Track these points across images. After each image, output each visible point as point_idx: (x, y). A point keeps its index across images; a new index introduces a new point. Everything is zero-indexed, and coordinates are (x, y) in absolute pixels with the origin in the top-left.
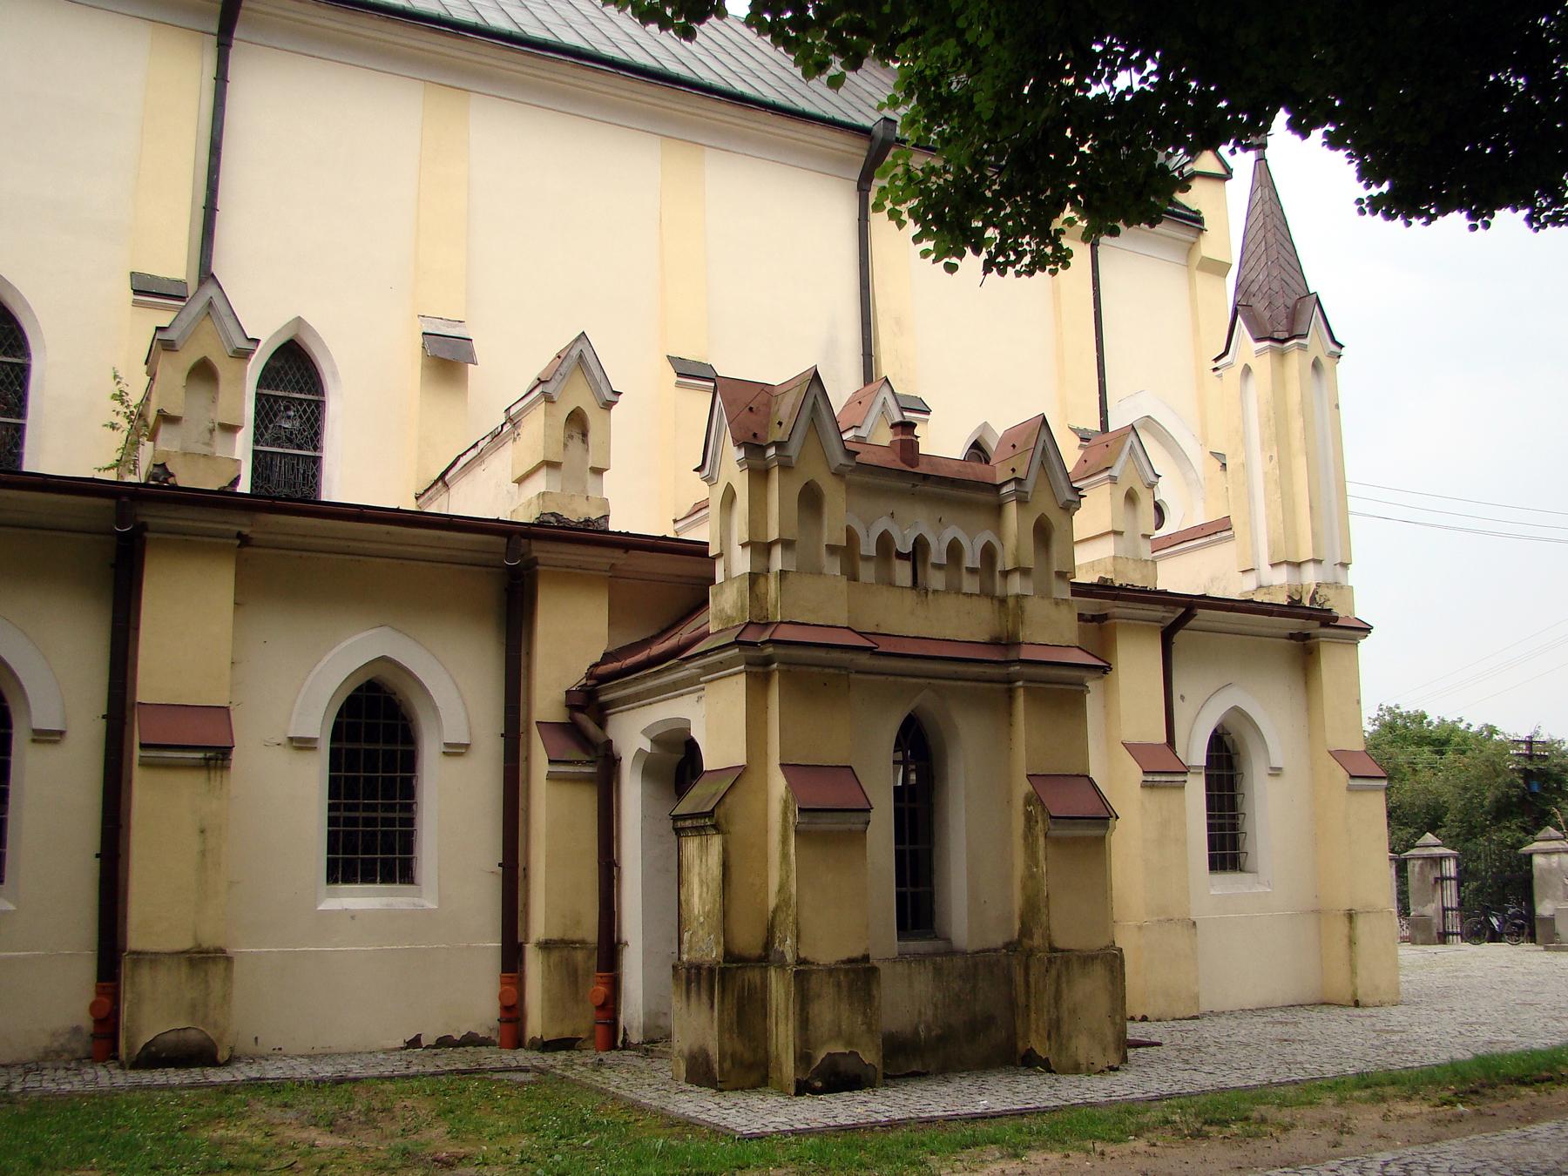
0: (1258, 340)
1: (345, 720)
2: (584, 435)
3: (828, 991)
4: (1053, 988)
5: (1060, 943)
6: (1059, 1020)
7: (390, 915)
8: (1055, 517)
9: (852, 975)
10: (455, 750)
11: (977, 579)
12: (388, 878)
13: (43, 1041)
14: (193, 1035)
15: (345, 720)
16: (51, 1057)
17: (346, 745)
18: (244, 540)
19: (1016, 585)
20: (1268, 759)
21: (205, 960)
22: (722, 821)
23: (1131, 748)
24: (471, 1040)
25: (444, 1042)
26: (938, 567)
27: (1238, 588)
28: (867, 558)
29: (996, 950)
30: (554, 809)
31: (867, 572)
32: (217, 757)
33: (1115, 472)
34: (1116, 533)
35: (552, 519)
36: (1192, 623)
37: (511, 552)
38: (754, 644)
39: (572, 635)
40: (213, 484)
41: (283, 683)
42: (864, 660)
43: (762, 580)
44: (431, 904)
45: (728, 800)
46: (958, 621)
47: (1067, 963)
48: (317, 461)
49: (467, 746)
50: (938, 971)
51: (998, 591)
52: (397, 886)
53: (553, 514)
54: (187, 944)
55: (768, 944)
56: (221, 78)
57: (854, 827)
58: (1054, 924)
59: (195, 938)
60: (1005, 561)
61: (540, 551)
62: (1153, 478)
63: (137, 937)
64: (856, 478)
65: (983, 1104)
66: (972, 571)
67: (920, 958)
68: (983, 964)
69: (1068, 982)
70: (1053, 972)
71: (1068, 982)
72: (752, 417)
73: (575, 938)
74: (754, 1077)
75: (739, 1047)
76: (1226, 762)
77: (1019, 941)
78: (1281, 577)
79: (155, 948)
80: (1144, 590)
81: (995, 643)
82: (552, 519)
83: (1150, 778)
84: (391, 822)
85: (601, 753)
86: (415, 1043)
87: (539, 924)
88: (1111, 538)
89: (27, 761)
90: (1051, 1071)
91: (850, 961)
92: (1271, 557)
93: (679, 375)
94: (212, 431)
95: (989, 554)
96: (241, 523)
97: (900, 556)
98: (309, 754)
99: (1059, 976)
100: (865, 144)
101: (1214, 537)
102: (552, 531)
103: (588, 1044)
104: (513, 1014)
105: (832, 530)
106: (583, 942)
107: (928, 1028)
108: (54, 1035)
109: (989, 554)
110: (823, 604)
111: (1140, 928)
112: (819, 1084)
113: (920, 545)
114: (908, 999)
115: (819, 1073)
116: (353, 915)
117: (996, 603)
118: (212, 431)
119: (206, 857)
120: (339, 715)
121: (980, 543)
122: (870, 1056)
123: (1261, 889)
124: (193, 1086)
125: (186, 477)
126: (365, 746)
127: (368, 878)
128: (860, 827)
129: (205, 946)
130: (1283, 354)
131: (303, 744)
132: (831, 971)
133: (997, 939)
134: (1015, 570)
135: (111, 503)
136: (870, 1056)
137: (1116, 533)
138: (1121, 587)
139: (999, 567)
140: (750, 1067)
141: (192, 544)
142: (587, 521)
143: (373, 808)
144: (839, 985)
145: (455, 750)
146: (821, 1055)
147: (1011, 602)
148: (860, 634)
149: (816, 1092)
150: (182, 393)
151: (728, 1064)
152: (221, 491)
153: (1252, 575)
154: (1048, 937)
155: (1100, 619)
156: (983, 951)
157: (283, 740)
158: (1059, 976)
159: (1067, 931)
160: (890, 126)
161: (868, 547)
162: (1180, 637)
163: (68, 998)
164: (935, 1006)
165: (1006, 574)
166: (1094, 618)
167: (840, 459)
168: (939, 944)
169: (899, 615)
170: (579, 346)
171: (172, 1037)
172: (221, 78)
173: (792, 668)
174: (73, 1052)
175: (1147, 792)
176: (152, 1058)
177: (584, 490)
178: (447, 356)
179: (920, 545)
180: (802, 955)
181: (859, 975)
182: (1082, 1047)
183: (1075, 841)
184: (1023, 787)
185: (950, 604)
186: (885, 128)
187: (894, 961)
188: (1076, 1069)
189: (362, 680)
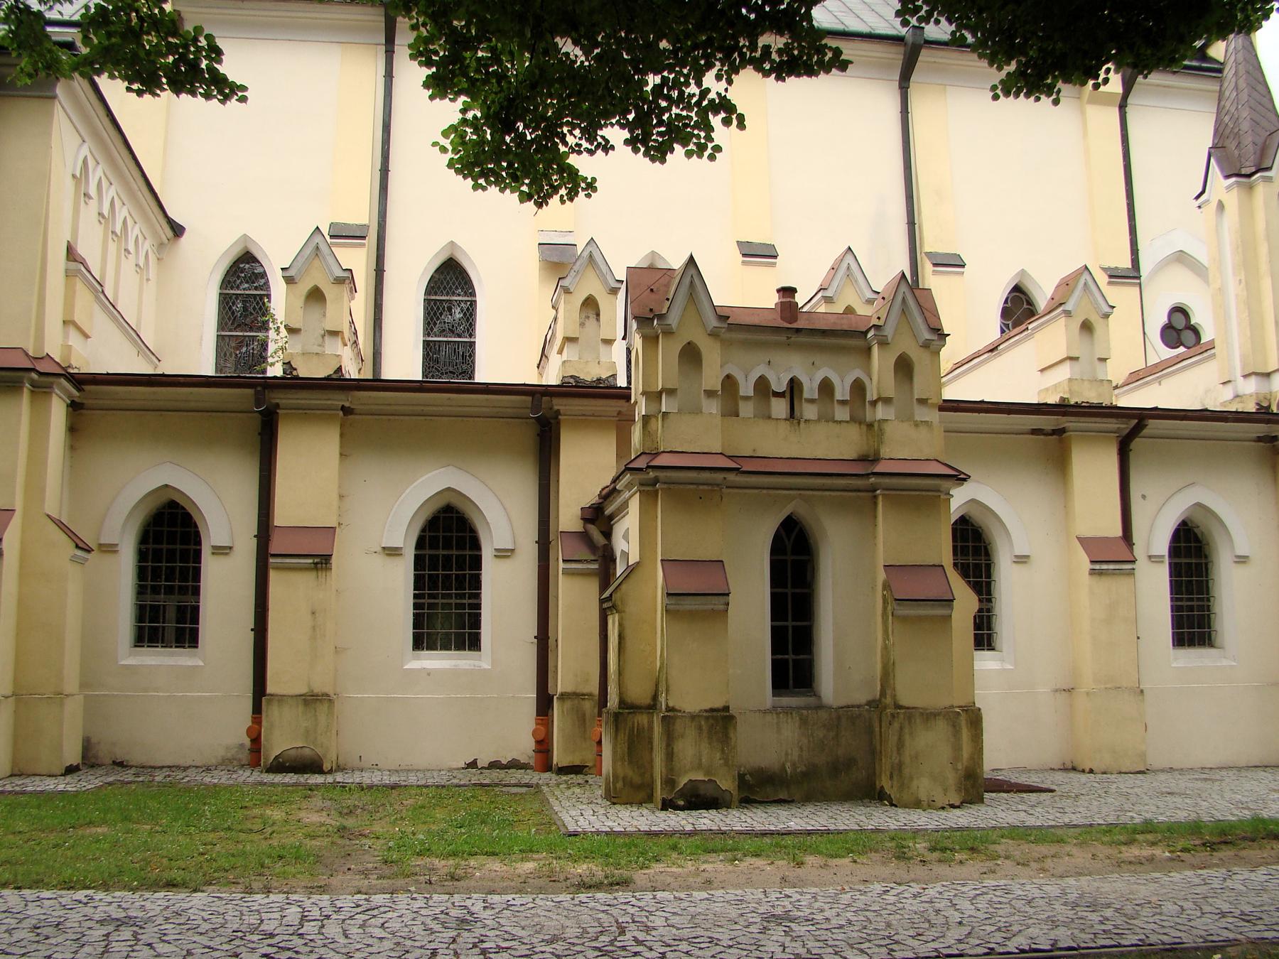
0: (1227, 177)
1: (427, 534)
2: (598, 315)
3: (691, 733)
4: (896, 738)
5: (905, 700)
6: (900, 765)
7: (455, 673)
8: (916, 354)
9: (711, 721)
10: (504, 554)
11: (847, 409)
12: (460, 647)
13: (221, 753)
14: (307, 752)
15: (427, 534)
16: (227, 763)
17: (428, 552)
18: (347, 411)
19: (881, 412)
20: (1233, 547)
21: (312, 700)
22: (619, 603)
23: (1082, 541)
24: (514, 765)
25: (494, 765)
26: (812, 401)
27: (1219, 400)
28: (747, 398)
29: (859, 706)
30: (575, 597)
31: (746, 409)
32: (322, 562)
33: (1068, 307)
34: (1071, 359)
35: (572, 380)
36: (1145, 432)
37: (536, 407)
38: (641, 469)
39: (586, 466)
40: (321, 374)
41: (372, 511)
42: (732, 477)
43: (653, 420)
44: (486, 665)
45: (624, 587)
46: (829, 442)
47: (910, 718)
48: (472, 344)
49: (512, 550)
50: (804, 722)
51: (869, 419)
52: (467, 653)
53: (572, 377)
54: (304, 690)
55: (655, 697)
56: (389, 75)
57: (716, 607)
58: (898, 687)
59: (309, 686)
60: (871, 394)
61: (558, 404)
62: (1107, 309)
63: (270, 689)
64: (728, 335)
65: (794, 824)
66: (843, 402)
67: (788, 710)
68: (846, 716)
69: (911, 734)
70: (896, 725)
71: (911, 734)
72: (653, 296)
73: (585, 691)
74: (642, 795)
75: (630, 773)
76: (1191, 554)
77: (880, 700)
78: (1250, 387)
79: (284, 692)
80: (1099, 406)
81: (863, 459)
82: (572, 380)
83: (1097, 567)
84: (462, 606)
85: (600, 553)
86: (473, 764)
87: (562, 682)
88: (1068, 363)
89: (211, 568)
90: (892, 805)
91: (712, 710)
92: (1243, 369)
93: (744, 255)
94: (323, 336)
95: (858, 388)
96: (340, 399)
97: (777, 394)
98: (397, 559)
99: (901, 728)
100: (901, 49)
101: (1205, 355)
102: (573, 389)
103: (593, 771)
104: (543, 746)
105: (712, 376)
106: (590, 695)
107: (794, 764)
108: (228, 748)
109: (858, 388)
110: (698, 434)
111: (1088, 694)
112: (681, 803)
113: (794, 385)
114: (770, 739)
115: (682, 794)
116: (429, 673)
117: (864, 427)
118: (323, 336)
119: (315, 631)
120: (423, 530)
121: (849, 380)
122: (727, 783)
123: (1225, 663)
124: (296, 785)
125: (305, 370)
126: (455, 552)
127: (446, 647)
128: (722, 607)
129: (315, 691)
130: (1251, 188)
131: (392, 552)
132: (693, 717)
133: (861, 697)
134: (879, 399)
135: (250, 391)
136: (727, 783)
137: (1071, 359)
138: (1077, 405)
139: (869, 398)
140: (638, 788)
141: (308, 415)
142: (599, 380)
143: (450, 596)
144: (700, 728)
145: (504, 554)
146: (683, 781)
147: (876, 425)
148: (729, 457)
149: (678, 808)
150: (301, 312)
151: (620, 785)
152: (328, 378)
153: (1229, 386)
154: (894, 697)
155: (1060, 432)
156: (848, 707)
157: (379, 549)
158: (901, 728)
159: (909, 692)
160: (918, 32)
161: (747, 389)
162: (1136, 444)
163: (232, 726)
164: (801, 748)
165: (874, 403)
166: (1054, 432)
167: (713, 322)
168: (811, 700)
169: (772, 440)
170: (589, 249)
171: (293, 752)
172: (389, 75)
173: (672, 486)
174: (240, 760)
175: (1096, 578)
176: (279, 767)
177: (598, 357)
178: (555, 260)
179: (794, 385)
180: (671, 704)
181: (720, 721)
182: (923, 787)
183: (920, 619)
184: (881, 576)
185: (822, 430)
186: (914, 34)
187: (765, 712)
188: (917, 804)
189: (440, 503)
